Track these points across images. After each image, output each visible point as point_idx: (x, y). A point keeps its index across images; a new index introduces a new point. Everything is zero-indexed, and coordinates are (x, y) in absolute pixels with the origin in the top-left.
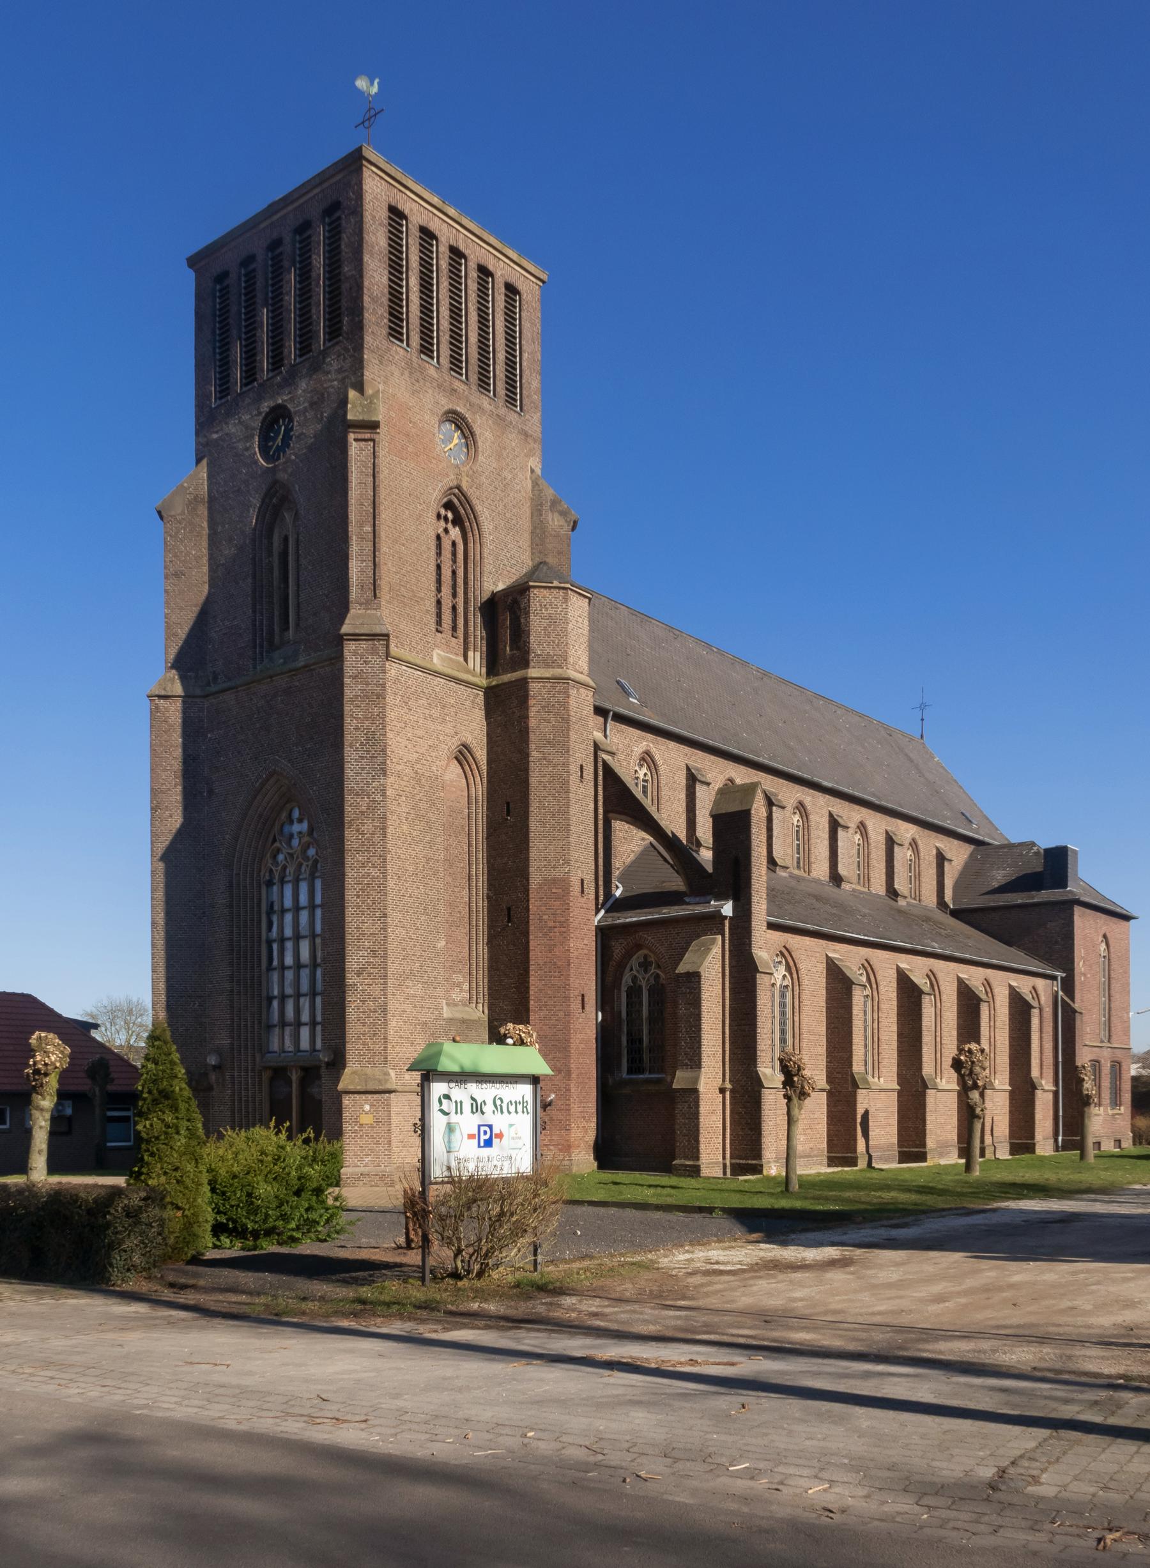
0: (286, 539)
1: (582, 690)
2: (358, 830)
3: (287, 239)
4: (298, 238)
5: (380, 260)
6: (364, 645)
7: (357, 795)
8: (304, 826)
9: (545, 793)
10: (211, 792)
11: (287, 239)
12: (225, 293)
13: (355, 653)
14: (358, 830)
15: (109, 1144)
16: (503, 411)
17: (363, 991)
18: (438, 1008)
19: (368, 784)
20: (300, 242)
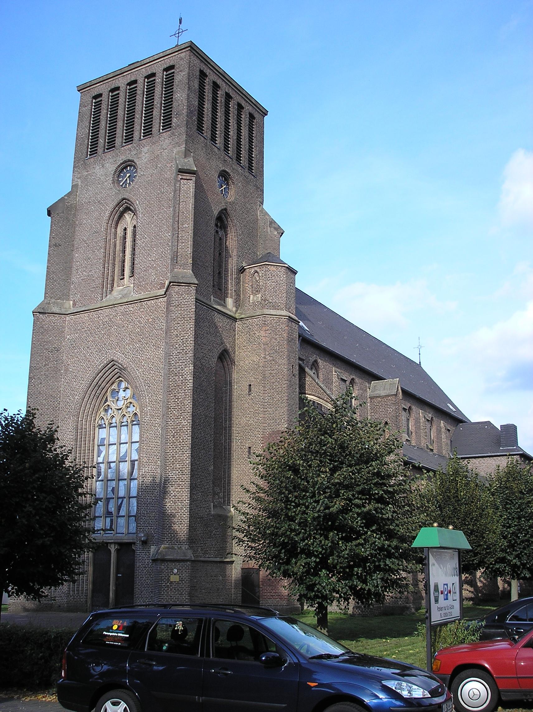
0: (125, 229)
1: (293, 324)
2: (175, 396)
3: (140, 81)
4: (94, 101)
5: (195, 94)
6: (183, 289)
7: (176, 375)
8: (129, 393)
9: (273, 380)
10: (67, 370)
11: (140, 81)
12: (98, 105)
13: (177, 293)
14: (175, 396)
15: (128, 636)
16: (247, 174)
17: (175, 496)
18: (209, 508)
19: (182, 369)
20: (95, 103)
